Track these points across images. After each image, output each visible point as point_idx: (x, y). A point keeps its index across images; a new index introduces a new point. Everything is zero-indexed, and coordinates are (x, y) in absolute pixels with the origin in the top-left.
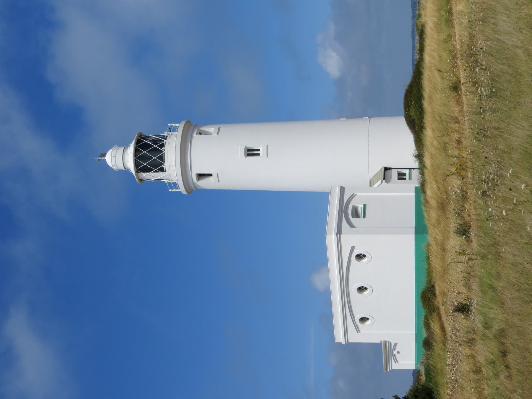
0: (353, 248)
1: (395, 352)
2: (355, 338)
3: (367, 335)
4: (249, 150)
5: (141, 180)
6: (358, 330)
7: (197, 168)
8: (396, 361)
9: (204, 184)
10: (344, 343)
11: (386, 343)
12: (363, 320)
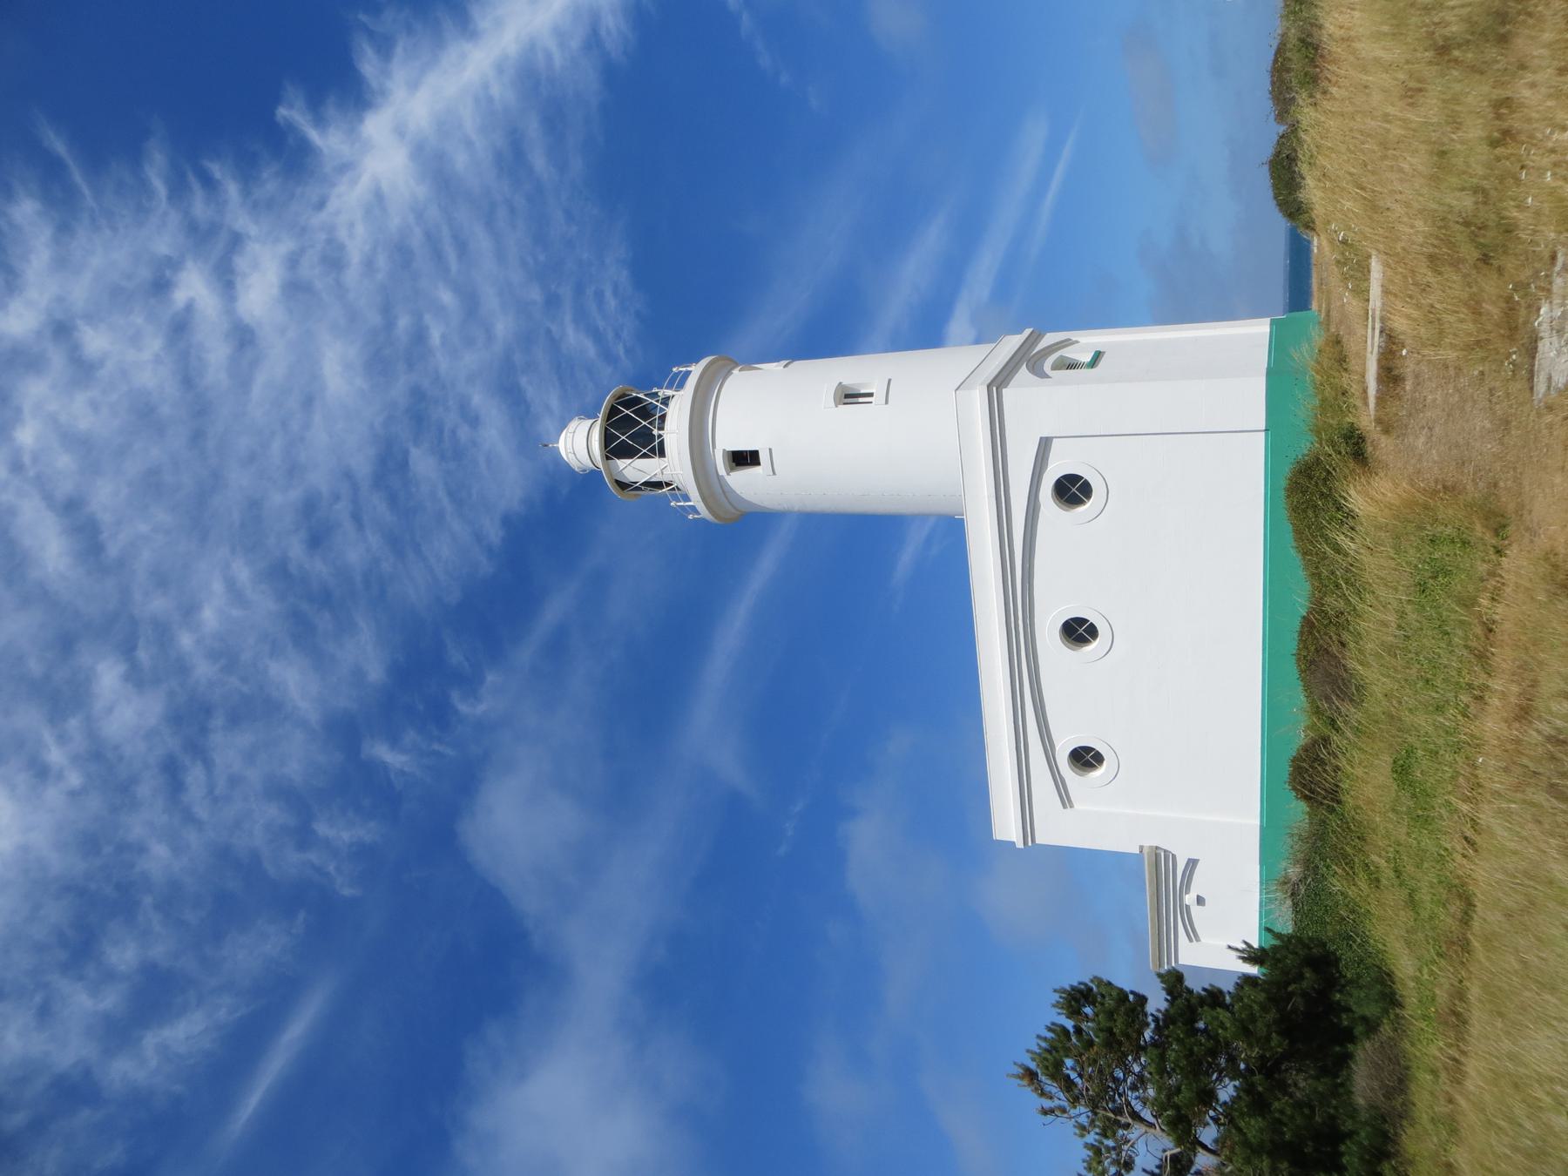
0: (1045, 445)
1: (1189, 899)
2: (1056, 828)
3: (1093, 819)
4: (847, 396)
5: (623, 485)
6: (1066, 800)
7: (729, 436)
8: (1193, 935)
9: (742, 482)
10: (1020, 845)
11: (1157, 856)
12: (1085, 758)
